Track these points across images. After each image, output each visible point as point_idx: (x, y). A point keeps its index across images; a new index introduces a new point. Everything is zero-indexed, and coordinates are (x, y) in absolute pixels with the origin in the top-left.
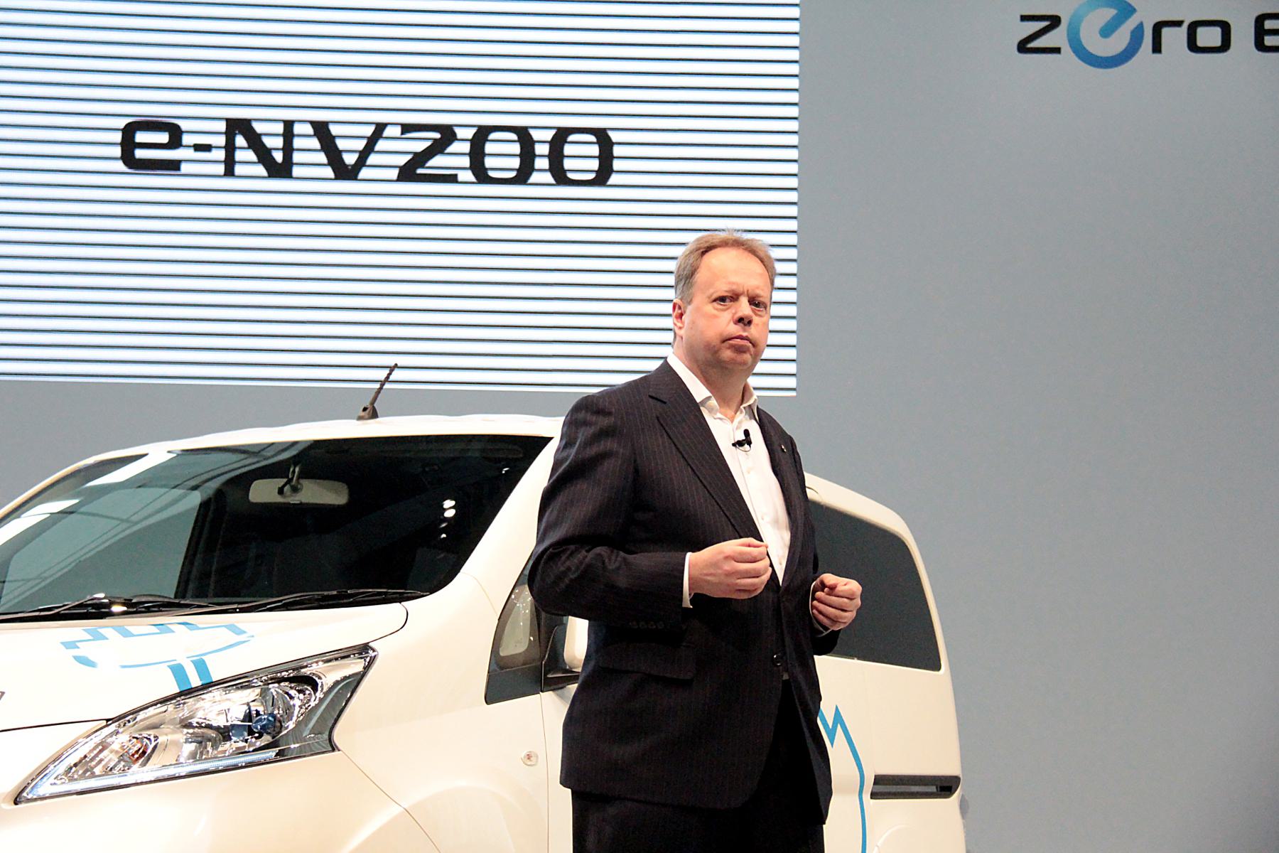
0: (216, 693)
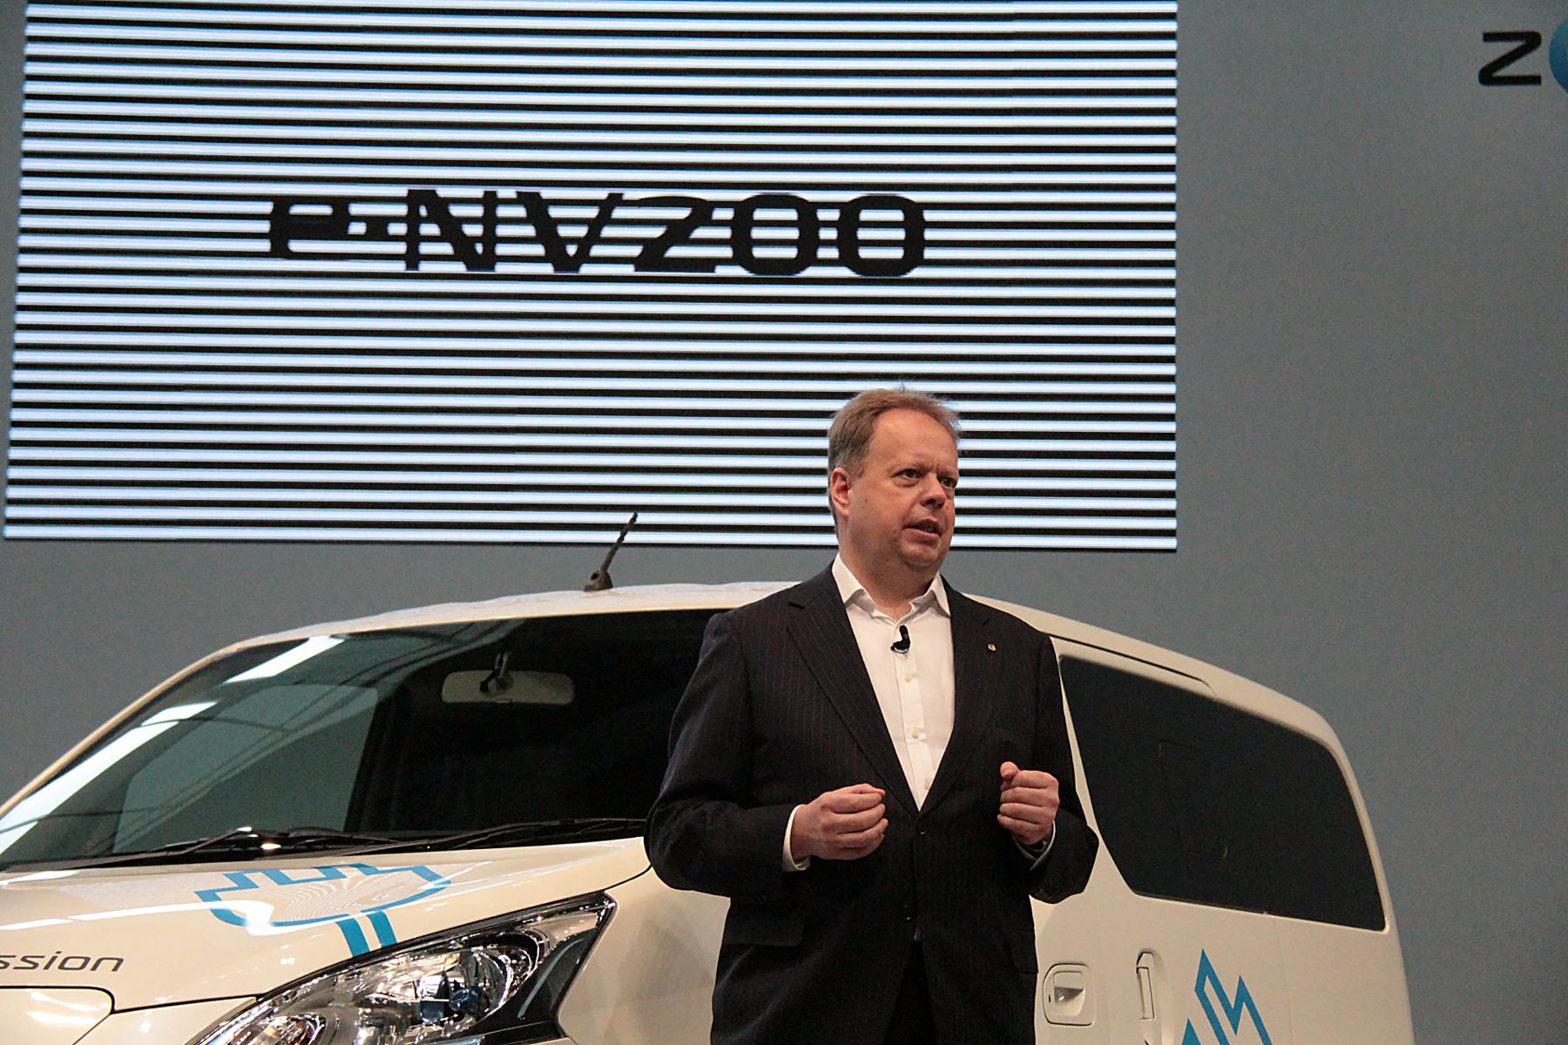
0: (401, 960)
